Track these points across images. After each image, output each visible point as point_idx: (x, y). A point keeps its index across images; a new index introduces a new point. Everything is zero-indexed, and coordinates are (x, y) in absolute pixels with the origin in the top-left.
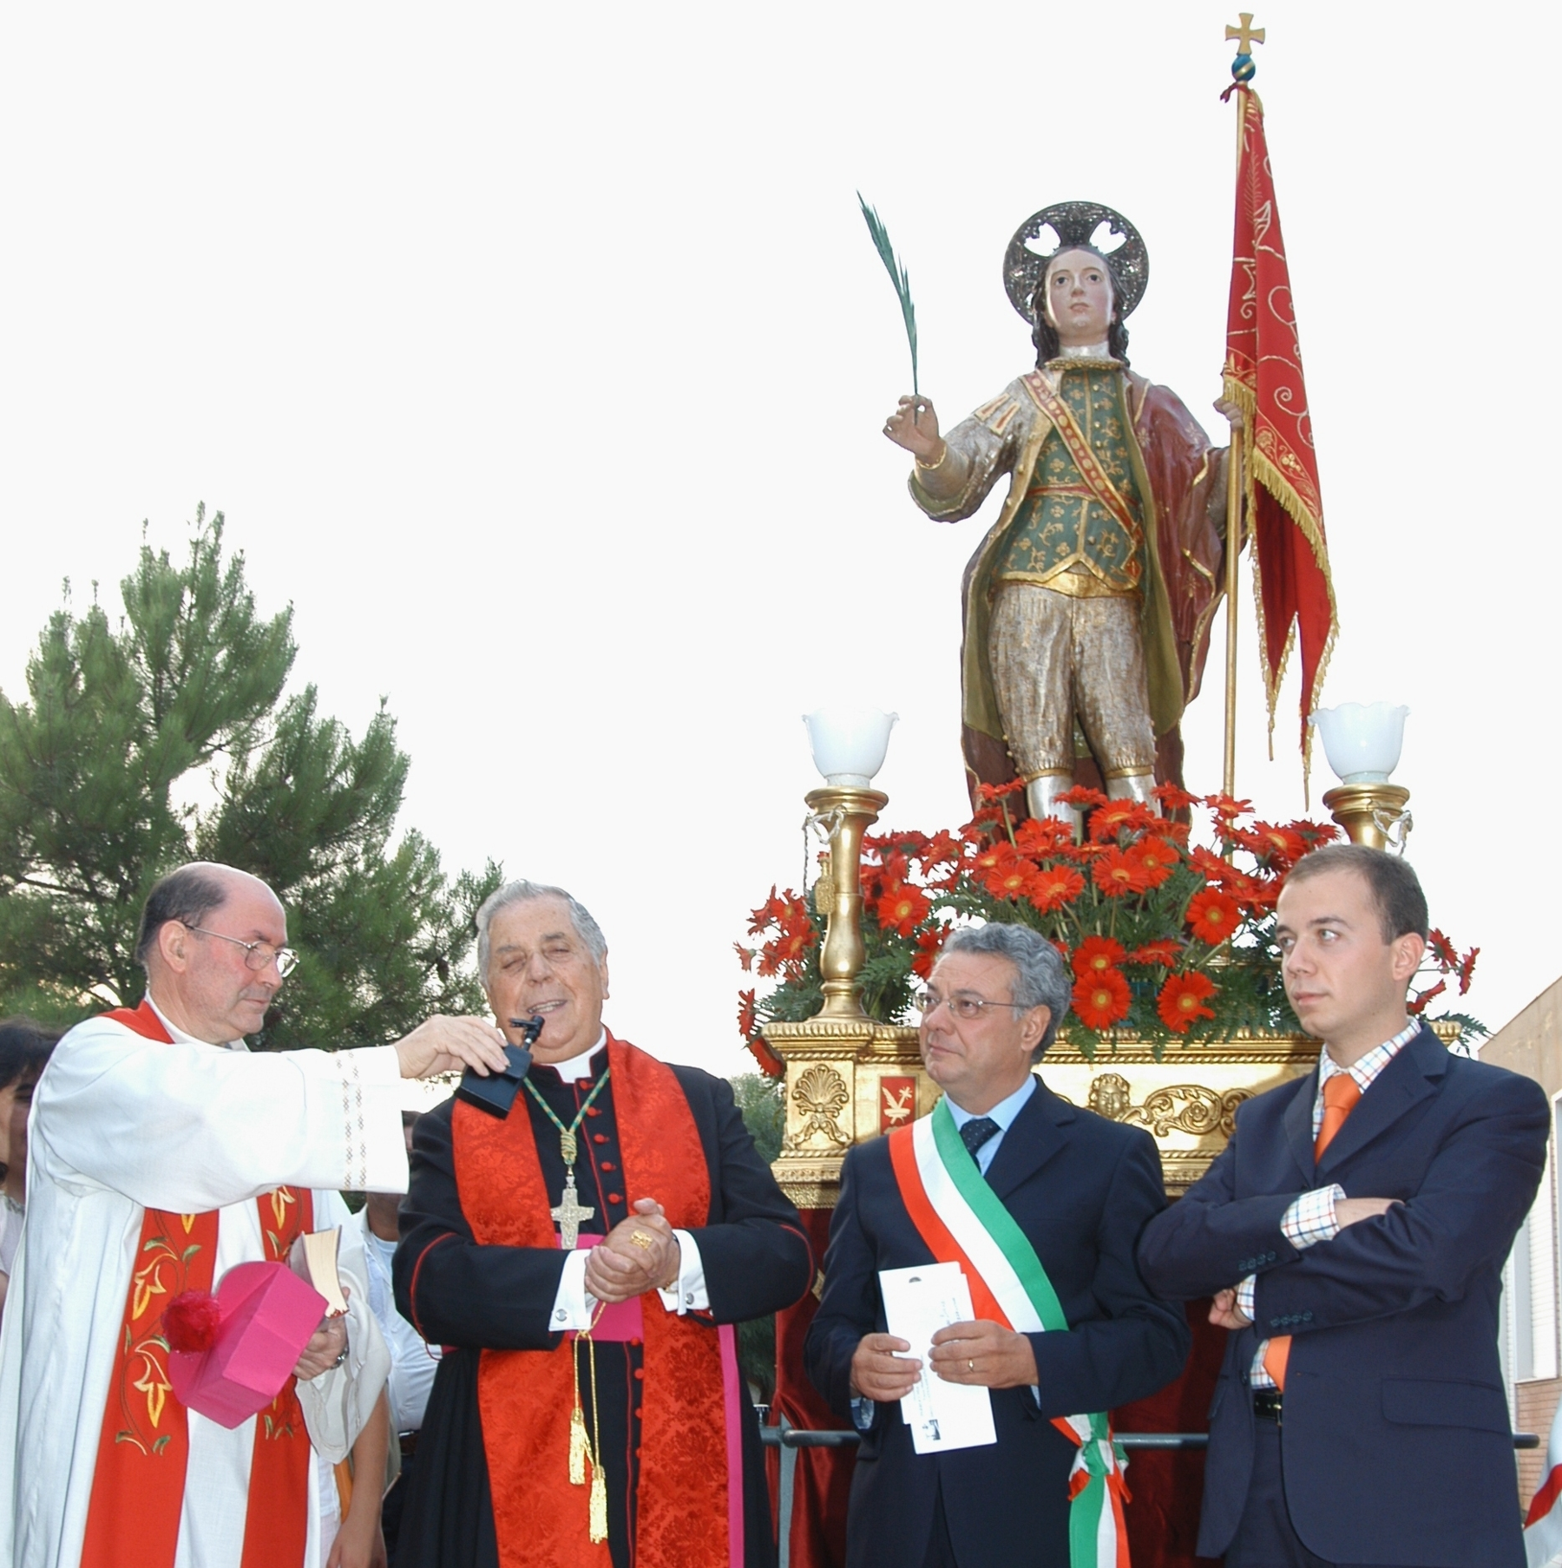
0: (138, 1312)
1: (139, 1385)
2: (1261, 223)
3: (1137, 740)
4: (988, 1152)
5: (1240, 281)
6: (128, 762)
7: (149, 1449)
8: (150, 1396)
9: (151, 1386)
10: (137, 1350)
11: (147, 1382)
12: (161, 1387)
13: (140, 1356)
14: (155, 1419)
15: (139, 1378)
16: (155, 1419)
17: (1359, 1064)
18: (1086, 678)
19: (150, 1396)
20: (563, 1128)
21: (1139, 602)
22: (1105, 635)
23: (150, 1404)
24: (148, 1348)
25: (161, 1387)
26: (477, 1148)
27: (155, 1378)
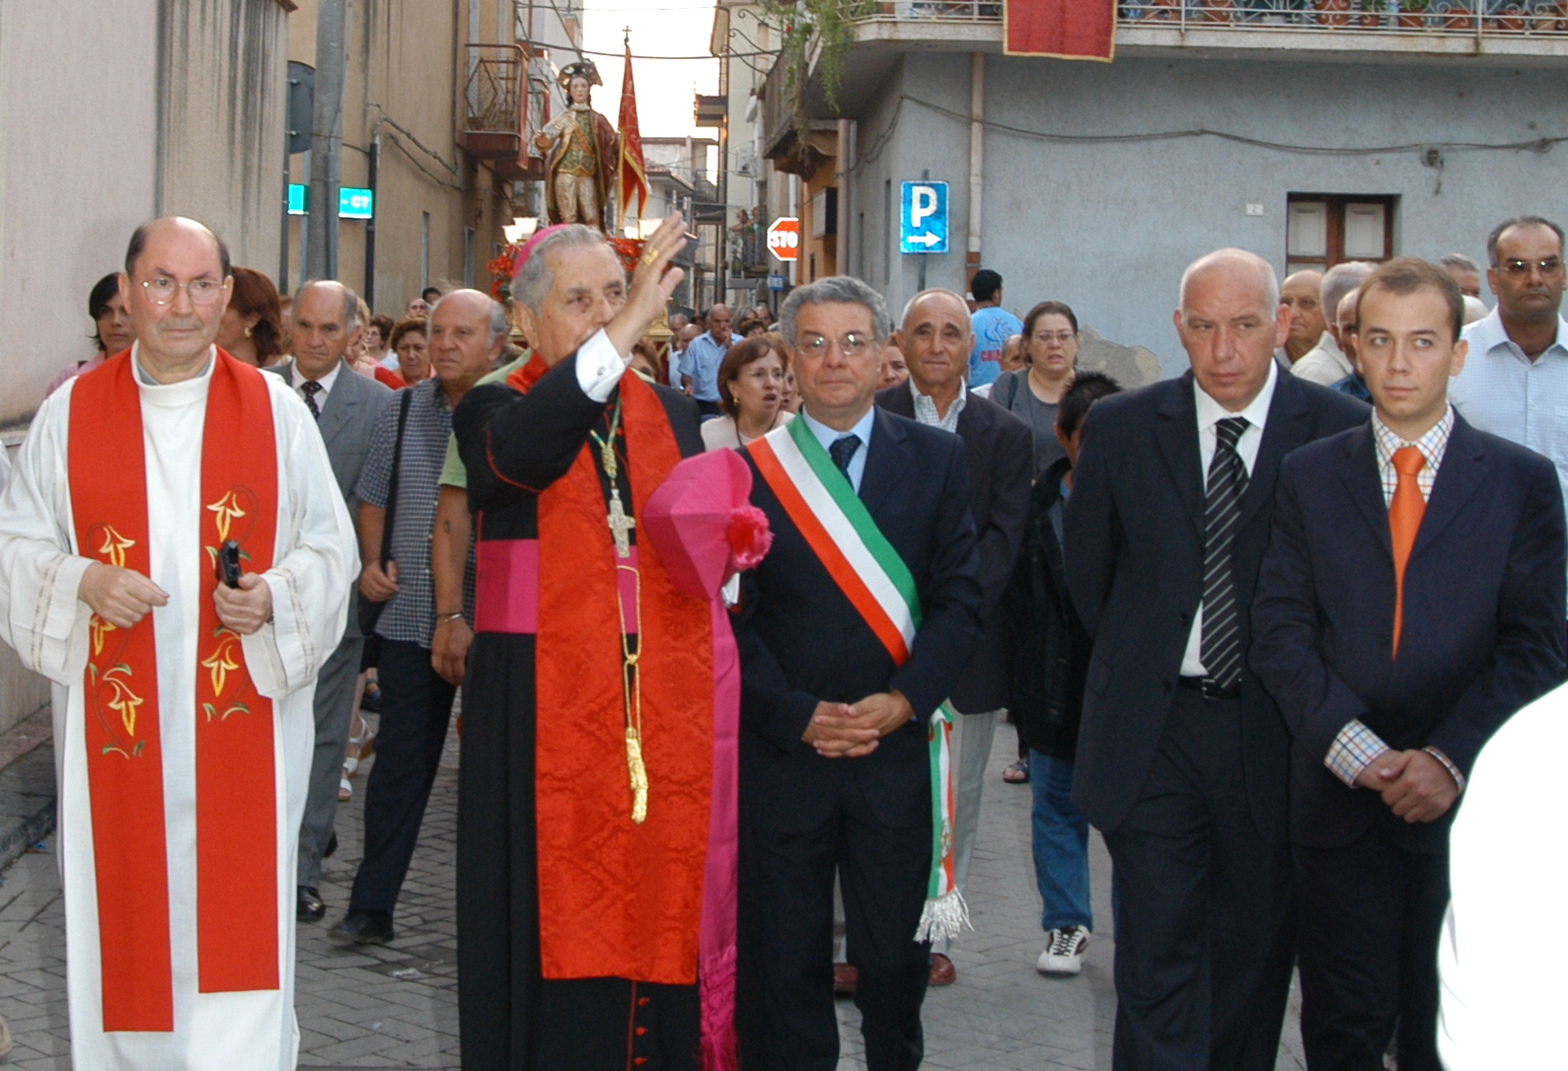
0: (98, 649)
1: (113, 705)
2: (629, 87)
3: (782, 128)
4: (857, 465)
5: (623, 99)
6: (648, 999)
7: (131, 755)
8: (124, 713)
9: (123, 704)
10: (105, 678)
11: (119, 702)
12: (131, 704)
13: (108, 682)
14: (130, 729)
15: (111, 700)
16: (130, 729)
17: (1424, 440)
18: (581, 199)
19: (124, 713)
20: (602, 443)
21: (595, 178)
22: (587, 189)
23: (125, 718)
24: (111, 675)
25: (131, 704)
26: (668, 930)
27: (125, 698)
